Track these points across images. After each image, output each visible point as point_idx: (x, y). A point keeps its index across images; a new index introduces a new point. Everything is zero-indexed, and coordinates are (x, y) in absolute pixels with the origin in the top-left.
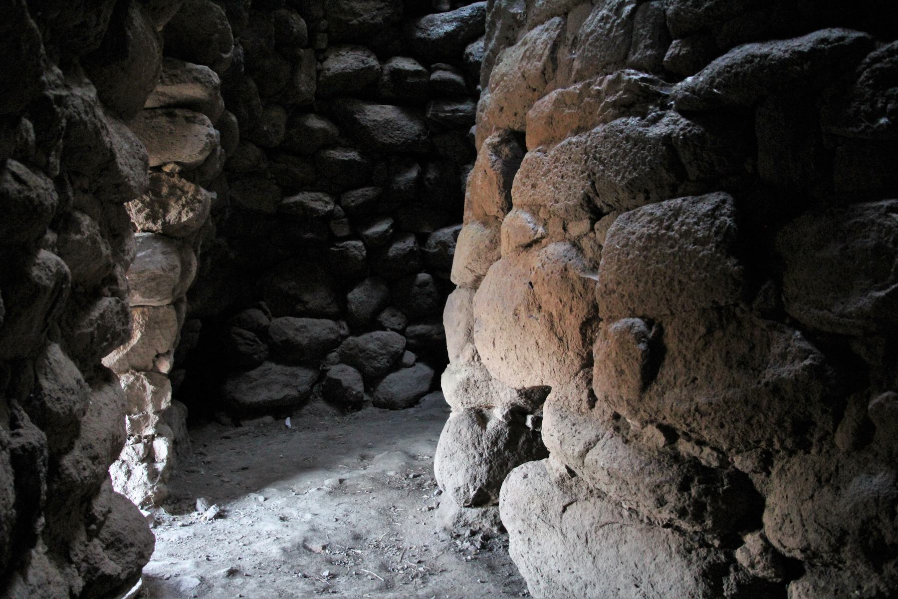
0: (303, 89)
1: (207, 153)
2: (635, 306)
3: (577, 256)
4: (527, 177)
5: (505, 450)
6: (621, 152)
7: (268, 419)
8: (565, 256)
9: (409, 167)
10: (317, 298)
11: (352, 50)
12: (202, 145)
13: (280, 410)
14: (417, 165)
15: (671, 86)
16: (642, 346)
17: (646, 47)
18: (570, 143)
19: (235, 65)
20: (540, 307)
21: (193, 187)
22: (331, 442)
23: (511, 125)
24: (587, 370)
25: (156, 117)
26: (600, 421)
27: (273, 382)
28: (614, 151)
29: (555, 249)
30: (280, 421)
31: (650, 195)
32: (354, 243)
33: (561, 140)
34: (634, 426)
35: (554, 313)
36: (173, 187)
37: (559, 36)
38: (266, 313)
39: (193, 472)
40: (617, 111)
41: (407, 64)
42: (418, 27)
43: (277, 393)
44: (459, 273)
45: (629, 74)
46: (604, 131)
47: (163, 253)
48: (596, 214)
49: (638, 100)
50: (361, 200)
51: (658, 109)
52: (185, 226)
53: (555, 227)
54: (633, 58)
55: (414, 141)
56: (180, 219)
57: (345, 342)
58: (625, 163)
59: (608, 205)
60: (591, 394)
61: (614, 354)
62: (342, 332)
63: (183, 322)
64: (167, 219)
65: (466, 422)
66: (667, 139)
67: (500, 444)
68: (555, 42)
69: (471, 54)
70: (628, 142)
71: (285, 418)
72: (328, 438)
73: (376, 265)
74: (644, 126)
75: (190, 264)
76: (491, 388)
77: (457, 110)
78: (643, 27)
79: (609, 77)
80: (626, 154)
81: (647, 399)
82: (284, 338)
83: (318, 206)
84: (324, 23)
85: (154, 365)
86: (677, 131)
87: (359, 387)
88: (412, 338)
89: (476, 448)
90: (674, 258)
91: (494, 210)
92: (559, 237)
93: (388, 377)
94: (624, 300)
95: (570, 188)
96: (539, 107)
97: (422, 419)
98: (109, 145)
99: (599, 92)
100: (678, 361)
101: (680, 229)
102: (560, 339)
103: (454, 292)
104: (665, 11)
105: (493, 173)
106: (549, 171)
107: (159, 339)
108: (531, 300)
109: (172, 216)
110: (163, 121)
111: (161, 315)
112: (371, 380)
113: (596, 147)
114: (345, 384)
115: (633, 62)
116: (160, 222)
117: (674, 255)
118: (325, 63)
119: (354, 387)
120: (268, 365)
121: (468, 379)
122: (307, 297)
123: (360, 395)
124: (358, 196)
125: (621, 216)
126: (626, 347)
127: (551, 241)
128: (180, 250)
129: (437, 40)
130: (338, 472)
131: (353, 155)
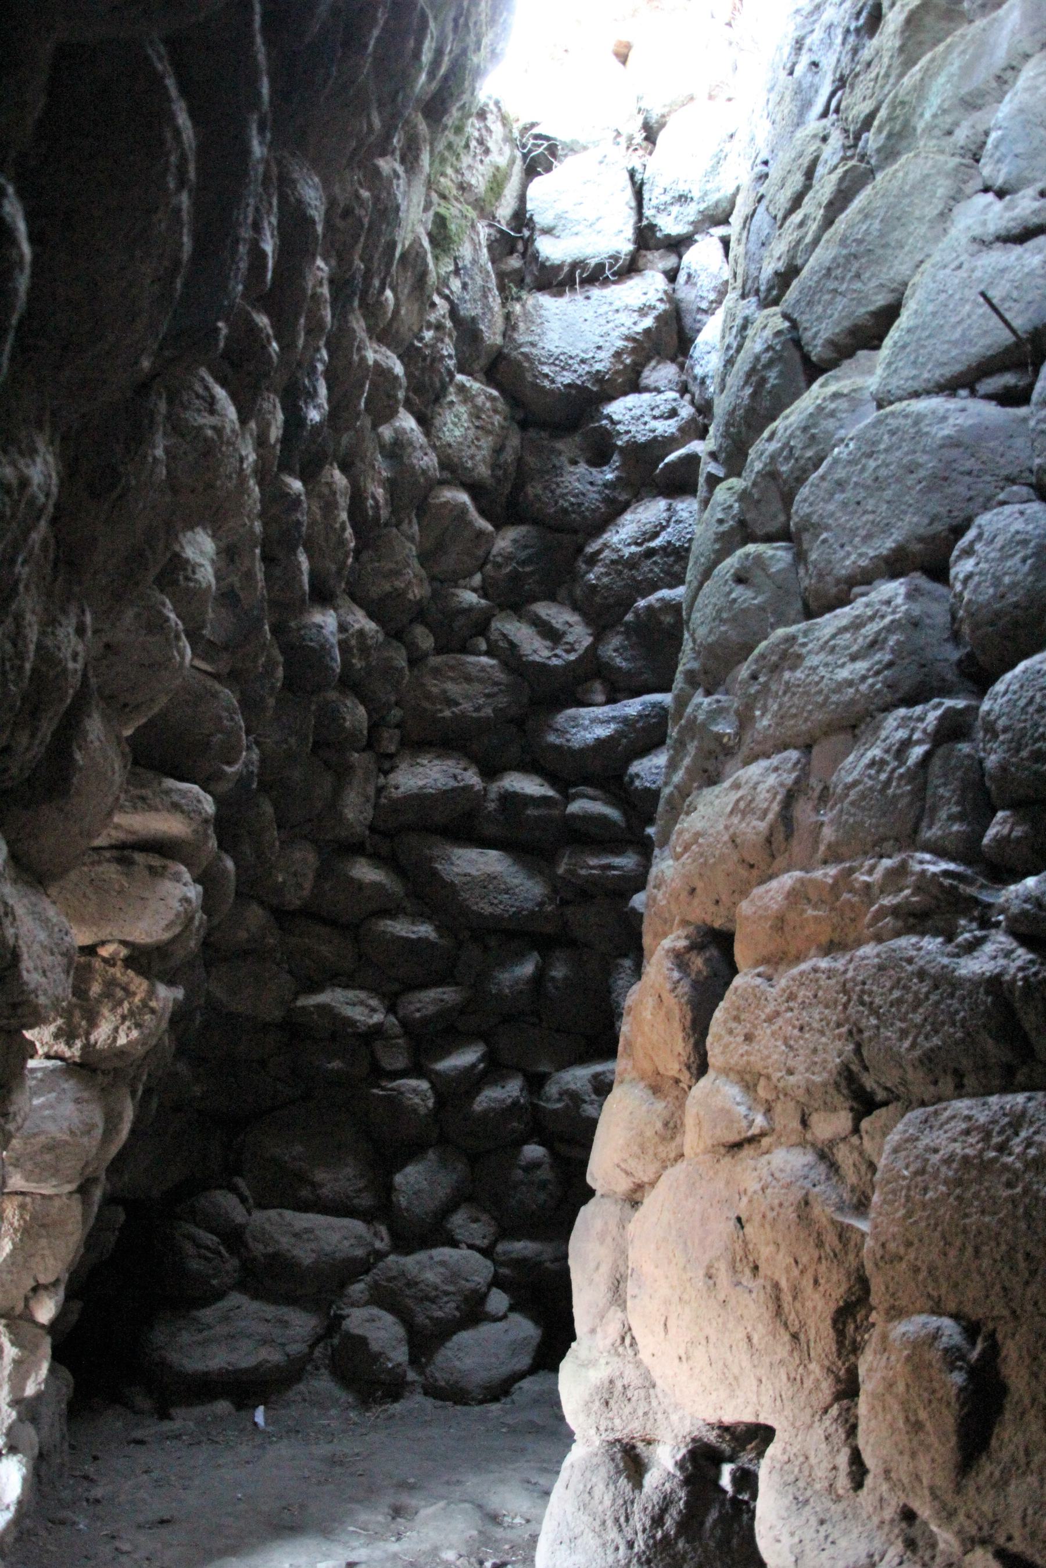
0: (350, 816)
1: (177, 930)
2: (943, 1291)
3: (828, 1179)
4: (737, 1019)
5: (678, 1535)
6: (910, 997)
7: (223, 1406)
8: (806, 1177)
9: (519, 957)
10: (340, 1179)
11: (438, 757)
12: (171, 916)
13: (247, 1389)
14: (536, 953)
15: (999, 890)
16: (958, 1378)
17: (952, 818)
18: (815, 970)
19: (243, 781)
20: (756, 1268)
21: (145, 985)
22: (338, 1470)
23: (708, 920)
24: (845, 1402)
25: (99, 863)
26: (876, 1520)
27: (241, 1333)
28: (896, 994)
29: (788, 1161)
30: (243, 1413)
31: (966, 1081)
32: (413, 1083)
33: (798, 959)
34: (946, 1542)
35: (784, 1284)
36: (111, 984)
37: (797, 781)
38: (243, 1200)
39: (63, 1523)
40: (900, 924)
41: (530, 786)
42: (550, 727)
43: (246, 1356)
44: (606, 1163)
45: (921, 862)
46: (878, 955)
47: (77, 1101)
48: (865, 1104)
49: (938, 907)
50: (431, 1009)
51: (974, 925)
52: (122, 1053)
53: (787, 1119)
54: (929, 834)
55: (532, 913)
56: (115, 1039)
57: (381, 1265)
58: (918, 1018)
59: (886, 1089)
60: (856, 1458)
61: (901, 1387)
62: (378, 1245)
63: (91, 1221)
64: (92, 1038)
65: (603, 1472)
66: (994, 983)
67: (669, 1522)
68: (789, 791)
69: (637, 775)
70: (922, 981)
71: (256, 1407)
72: (333, 1461)
73: (450, 1123)
74: (951, 955)
75: (120, 1116)
76: (654, 1403)
77: (610, 867)
78: (945, 784)
79: (887, 863)
80: (917, 1004)
81: (972, 1491)
82: (270, 1250)
83: (357, 1014)
84: (396, 714)
85: (27, 1306)
86: (1012, 971)
87: (400, 1355)
88: (502, 1264)
89: (621, 1531)
90: (1015, 1207)
91: (673, 1067)
92: (794, 1138)
93: (455, 1338)
94: (920, 1278)
95: (815, 1051)
96: (761, 898)
97: (513, 1430)
98: (11, 942)
99: (868, 886)
100: (1030, 1416)
101: (1024, 1153)
102: (795, 1337)
103: (592, 1201)
104: (981, 761)
105: (674, 1001)
106: (777, 1014)
107: (43, 1257)
108: (740, 1253)
109: (101, 1034)
110: (111, 871)
111: (54, 1211)
112: (424, 1342)
113: (864, 983)
114: (375, 1347)
115: (929, 839)
116: (78, 1044)
117: (1013, 1201)
118: (391, 776)
119: (392, 1355)
120: (236, 1298)
121: (611, 1382)
122: (320, 1175)
123: (399, 1370)
124: (429, 1000)
125: (909, 1115)
126: (925, 1373)
127: (779, 1144)
128: (105, 1091)
129: (581, 751)
130: (345, 1544)
131: (425, 930)
